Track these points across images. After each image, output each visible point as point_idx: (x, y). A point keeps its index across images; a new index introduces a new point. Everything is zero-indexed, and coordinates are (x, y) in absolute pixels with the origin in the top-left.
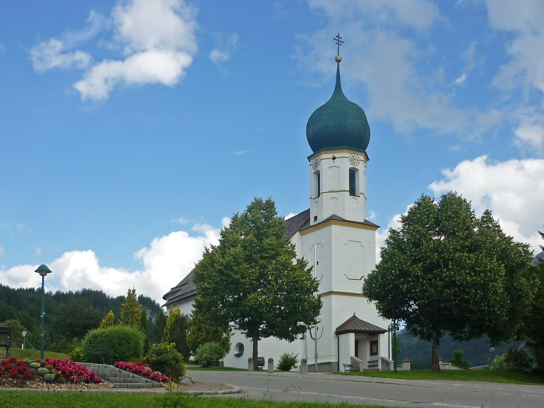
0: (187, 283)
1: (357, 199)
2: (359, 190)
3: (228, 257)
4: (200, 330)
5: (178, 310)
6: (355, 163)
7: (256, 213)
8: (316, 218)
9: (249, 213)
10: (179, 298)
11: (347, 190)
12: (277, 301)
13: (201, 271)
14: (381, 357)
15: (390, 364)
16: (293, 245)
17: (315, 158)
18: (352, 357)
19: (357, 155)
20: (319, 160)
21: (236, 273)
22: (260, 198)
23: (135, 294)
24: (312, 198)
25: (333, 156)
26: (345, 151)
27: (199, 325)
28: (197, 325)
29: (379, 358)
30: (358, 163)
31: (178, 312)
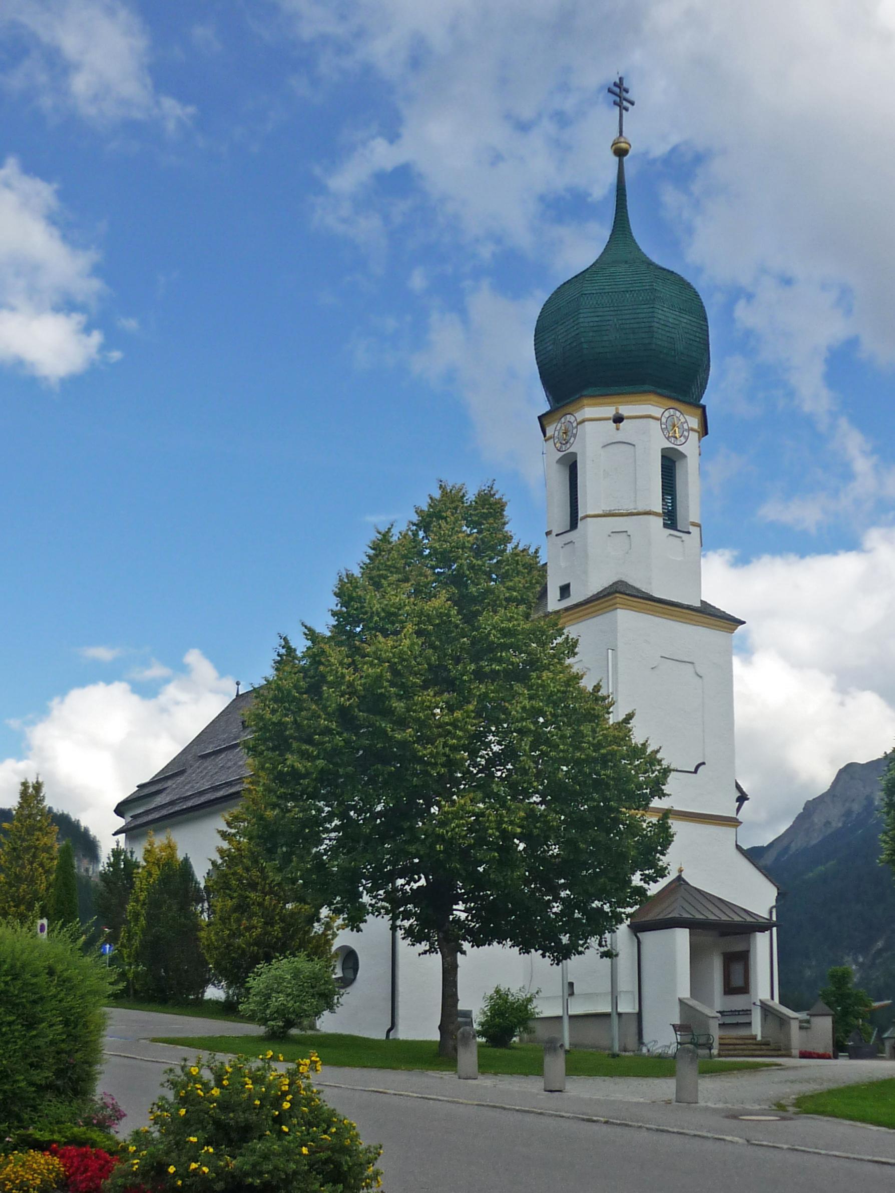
0: (181, 773)
1: (683, 539)
2: (688, 516)
3: (372, 665)
4: (246, 911)
5: (171, 847)
6: (676, 438)
7: (453, 529)
8: (565, 591)
9: (421, 534)
10: (164, 812)
11: (655, 510)
12: (538, 825)
13: (274, 712)
14: (760, 1001)
15: (789, 1023)
16: (572, 639)
17: (563, 420)
18: (686, 1001)
19: (681, 413)
20: (575, 424)
21: (401, 723)
22: (457, 486)
23: (42, 795)
24: (554, 534)
25: (614, 412)
26: (650, 400)
27: (240, 895)
28: (235, 895)
29: (754, 1004)
30: (685, 436)
31: (169, 850)
